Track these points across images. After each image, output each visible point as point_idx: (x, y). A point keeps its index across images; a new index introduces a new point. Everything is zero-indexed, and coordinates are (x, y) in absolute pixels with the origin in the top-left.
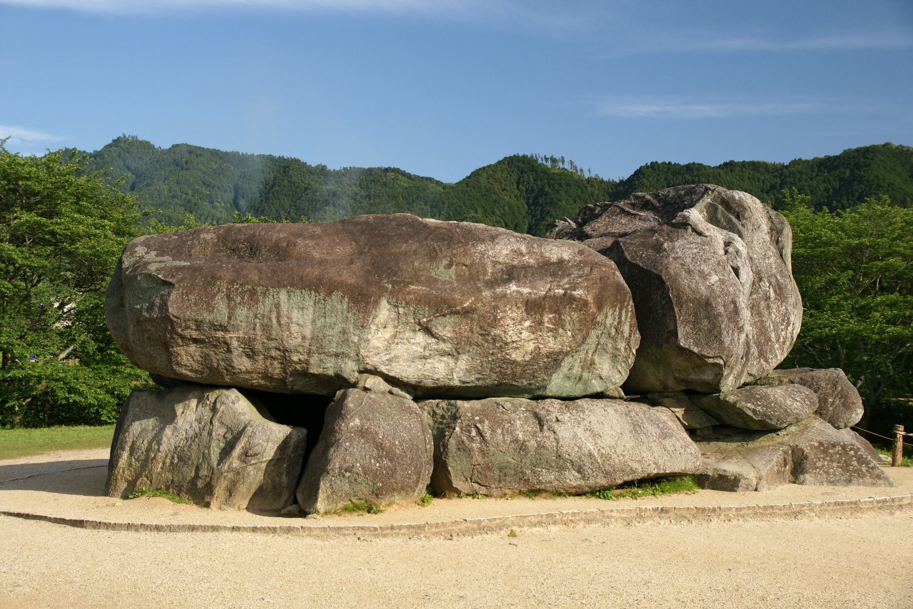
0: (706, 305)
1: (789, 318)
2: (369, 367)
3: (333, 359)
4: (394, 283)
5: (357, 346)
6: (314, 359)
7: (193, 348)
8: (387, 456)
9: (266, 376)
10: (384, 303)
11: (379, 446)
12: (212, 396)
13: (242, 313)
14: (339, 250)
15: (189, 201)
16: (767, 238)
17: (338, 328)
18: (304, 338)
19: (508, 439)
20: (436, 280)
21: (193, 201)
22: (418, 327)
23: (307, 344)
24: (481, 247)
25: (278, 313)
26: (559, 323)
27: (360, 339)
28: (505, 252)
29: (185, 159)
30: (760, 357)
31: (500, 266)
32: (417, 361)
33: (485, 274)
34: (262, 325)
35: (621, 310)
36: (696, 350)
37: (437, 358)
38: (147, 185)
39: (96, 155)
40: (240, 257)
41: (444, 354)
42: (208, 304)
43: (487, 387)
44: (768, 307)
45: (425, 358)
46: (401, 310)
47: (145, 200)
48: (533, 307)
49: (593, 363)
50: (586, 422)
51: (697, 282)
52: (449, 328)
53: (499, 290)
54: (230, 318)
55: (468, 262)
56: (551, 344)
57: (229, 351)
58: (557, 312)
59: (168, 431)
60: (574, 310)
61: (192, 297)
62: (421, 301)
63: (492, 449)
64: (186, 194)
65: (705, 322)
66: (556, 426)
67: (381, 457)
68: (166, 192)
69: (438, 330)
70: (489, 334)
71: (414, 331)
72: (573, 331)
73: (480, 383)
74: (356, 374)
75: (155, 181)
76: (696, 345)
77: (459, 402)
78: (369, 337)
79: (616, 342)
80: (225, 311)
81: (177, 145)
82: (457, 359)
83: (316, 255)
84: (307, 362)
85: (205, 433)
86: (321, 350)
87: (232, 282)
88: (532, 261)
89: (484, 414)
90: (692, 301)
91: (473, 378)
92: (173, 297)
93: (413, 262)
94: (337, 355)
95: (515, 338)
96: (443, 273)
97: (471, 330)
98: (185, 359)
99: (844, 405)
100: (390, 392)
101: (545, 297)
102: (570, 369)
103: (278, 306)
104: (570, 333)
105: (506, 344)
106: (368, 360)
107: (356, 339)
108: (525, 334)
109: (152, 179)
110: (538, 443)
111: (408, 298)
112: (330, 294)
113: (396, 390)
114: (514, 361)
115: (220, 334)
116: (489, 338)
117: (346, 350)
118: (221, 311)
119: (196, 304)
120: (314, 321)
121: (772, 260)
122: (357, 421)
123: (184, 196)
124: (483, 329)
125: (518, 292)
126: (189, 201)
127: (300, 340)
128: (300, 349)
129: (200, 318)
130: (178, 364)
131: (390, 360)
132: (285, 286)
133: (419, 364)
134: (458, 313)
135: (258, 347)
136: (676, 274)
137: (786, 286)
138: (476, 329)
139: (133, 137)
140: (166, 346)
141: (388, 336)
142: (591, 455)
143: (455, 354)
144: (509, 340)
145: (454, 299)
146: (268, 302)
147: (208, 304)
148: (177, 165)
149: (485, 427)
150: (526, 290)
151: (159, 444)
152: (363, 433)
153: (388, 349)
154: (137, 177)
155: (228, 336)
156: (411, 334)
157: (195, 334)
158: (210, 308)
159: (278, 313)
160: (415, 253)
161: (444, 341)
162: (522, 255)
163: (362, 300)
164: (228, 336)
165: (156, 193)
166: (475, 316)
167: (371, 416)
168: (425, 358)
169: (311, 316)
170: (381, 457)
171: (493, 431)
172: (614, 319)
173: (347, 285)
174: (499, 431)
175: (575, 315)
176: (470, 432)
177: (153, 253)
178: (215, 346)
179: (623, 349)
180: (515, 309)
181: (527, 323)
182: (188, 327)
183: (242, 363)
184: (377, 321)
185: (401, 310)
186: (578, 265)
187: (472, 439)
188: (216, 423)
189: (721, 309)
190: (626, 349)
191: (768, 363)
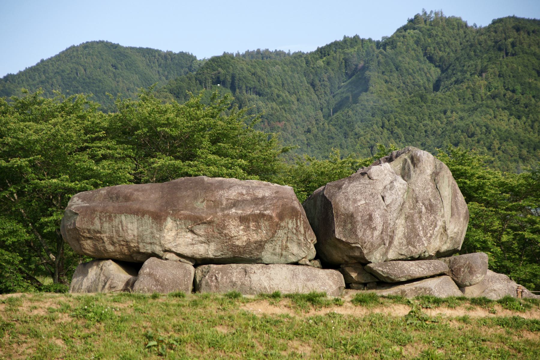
0: (351, 217)
1: (436, 223)
2: (167, 249)
3: (149, 245)
4: (173, 210)
5: (159, 239)
6: (141, 245)
7: (89, 241)
8: (160, 285)
9: (121, 253)
10: (169, 219)
11: (157, 281)
12: (102, 263)
13: (106, 225)
14: (152, 196)
15: (517, 102)
16: (429, 178)
17: (149, 231)
18: (134, 236)
19: (228, 281)
20: (196, 208)
21: (523, 101)
22: (188, 230)
23: (136, 239)
24: (221, 192)
25: (122, 225)
26: (258, 227)
27: (160, 236)
28: (234, 194)
29: (510, 40)
30: (408, 245)
31: (231, 201)
32: (190, 246)
33: (222, 204)
34: (116, 230)
35: (296, 220)
36: (344, 240)
37: (199, 244)
38: (456, 82)
39: (387, 43)
40: (113, 201)
41: (202, 242)
42: (92, 222)
43: (228, 258)
44: (421, 217)
45: (193, 244)
46: (178, 223)
47: (453, 103)
48: (243, 219)
49: (287, 247)
50: (269, 274)
51: (349, 205)
52: (202, 230)
53: (226, 212)
54: (101, 228)
55: (213, 199)
56: (255, 237)
57: (104, 242)
58: (257, 221)
59: (85, 280)
60: (266, 220)
61: (85, 219)
62: (187, 218)
63: (220, 285)
64: (514, 91)
65: (349, 226)
66: (251, 275)
67: (157, 285)
68: (483, 91)
69: (197, 231)
70: (222, 233)
71: (186, 232)
72: (267, 230)
73: (224, 256)
74: (162, 252)
75: (468, 75)
76: (344, 237)
77: (212, 265)
78: (165, 235)
79: (298, 236)
80: (99, 225)
81: (500, 20)
82: (209, 245)
83: (141, 199)
84: (138, 247)
85: (97, 279)
86: (143, 241)
87: (101, 212)
88: (248, 198)
89: (221, 270)
90: (344, 215)
91: (219, 254)
92: (78, 219)
93: (185, 201)
94: (151, 243)
95: (235, 234)
96: (201, 205)
97: (213, 231)
98: (87, 247)
99: (469, 272)
100: (180, 261)
101: (250, 215)
102: (274, 250)
103: (121, 222)
104: (265, 232)
105: (232, 237)
106: (166, 246)
107: (158, 236)
108: (241, 233)
109: (464, 72)
110: (242, 283)
111: (180, 217)
112: (143, 216)
113: (182, 260)
114: (238, 246)
115: (98, 235)
116: (223, 235)
117: (155, 241)
118: (97, 225)
119: (87, 222)
120: (138, 228)
121: (430, 190)
122: (148, 270)
123: (509, 94)
124: (218, 230)
125: (236, 213)
126: (517, 102)
127: (132, 237)
128: (134, 241)
129: (89, 228)
130: (84, 249)
131: (176, 246)
132: (123, 213)
133: (191, 248)
134: (205, 223)
135: (115, 240)
136: (339, 201)
137: (436, 205)
138: (216, 230)
139: (436, 14)
140: (78, 240)
141: (173, 234)
142: (265, 288)
143: (208, 242)
144: (233, 235)
145: (202, 217)
146: (117, 220)
147: (92, 222)
148: (500, 49)
149: (219, 277)
150: (240, 212)
151: (82, 286)
152: (150, 275)
153: (174, 240)
154: (443, 71)
155: (102, 236)
156: (185, 233)
157: (88, 235)
158: (93, 224)
159: (122, 225)
160: (188, 196)
161: (201, 236)
162: (243, 195)
163: (158, 218)
164: (102, 236)
165: (469, 94)
166: (214, 224)
167: (154, 268)
168: (193, 244)
169: (136, 226)
170: (157, 285)
171: (222, 277)
172: (294, 225)
173: (150, 212)
174: (225, 277)
175: (267, 223)
176: (212, 278)
177: (80, 200)
178: (98, 240)
179: (302, 240)
180: (234, 220)
181: (242, 227)
182: (84, 232)
183: (111, 248)
184: (167, 227)
185: (178, 223)
186: (272, 199)
187: (212, 281)
188: (102, 275)
189: (359, 218)
190: (304, 240)
191: (416, 248)
